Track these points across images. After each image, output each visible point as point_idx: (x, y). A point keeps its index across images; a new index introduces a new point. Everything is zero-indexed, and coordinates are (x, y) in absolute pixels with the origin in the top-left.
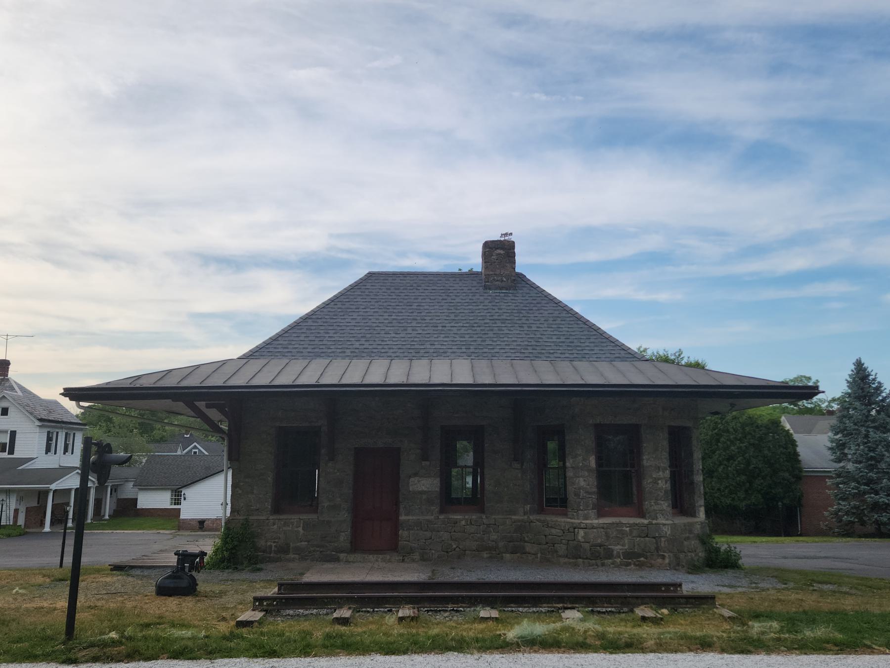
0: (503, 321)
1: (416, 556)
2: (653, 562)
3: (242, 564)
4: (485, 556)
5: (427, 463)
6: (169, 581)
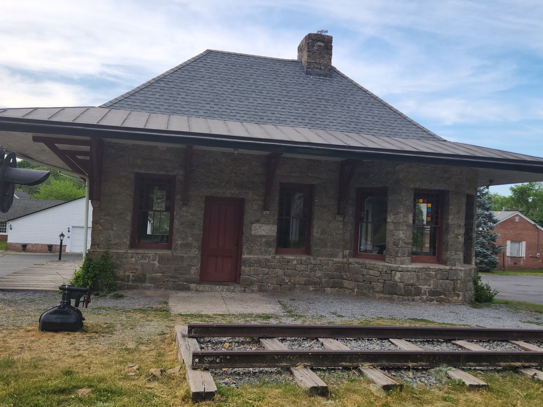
0: (327, 101)
1: (255, 288)
2: (450, 299)
3: (102, 290)
4: (311, 289)
5: (268, 212)
6: (54, 316)
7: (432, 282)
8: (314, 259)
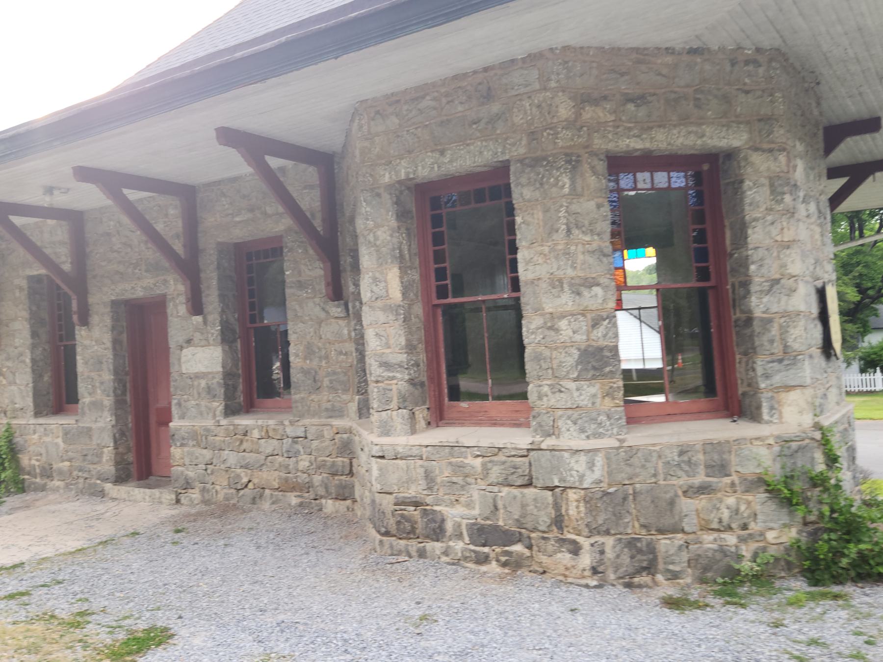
7: (476, 495)
8: (292, 423)
